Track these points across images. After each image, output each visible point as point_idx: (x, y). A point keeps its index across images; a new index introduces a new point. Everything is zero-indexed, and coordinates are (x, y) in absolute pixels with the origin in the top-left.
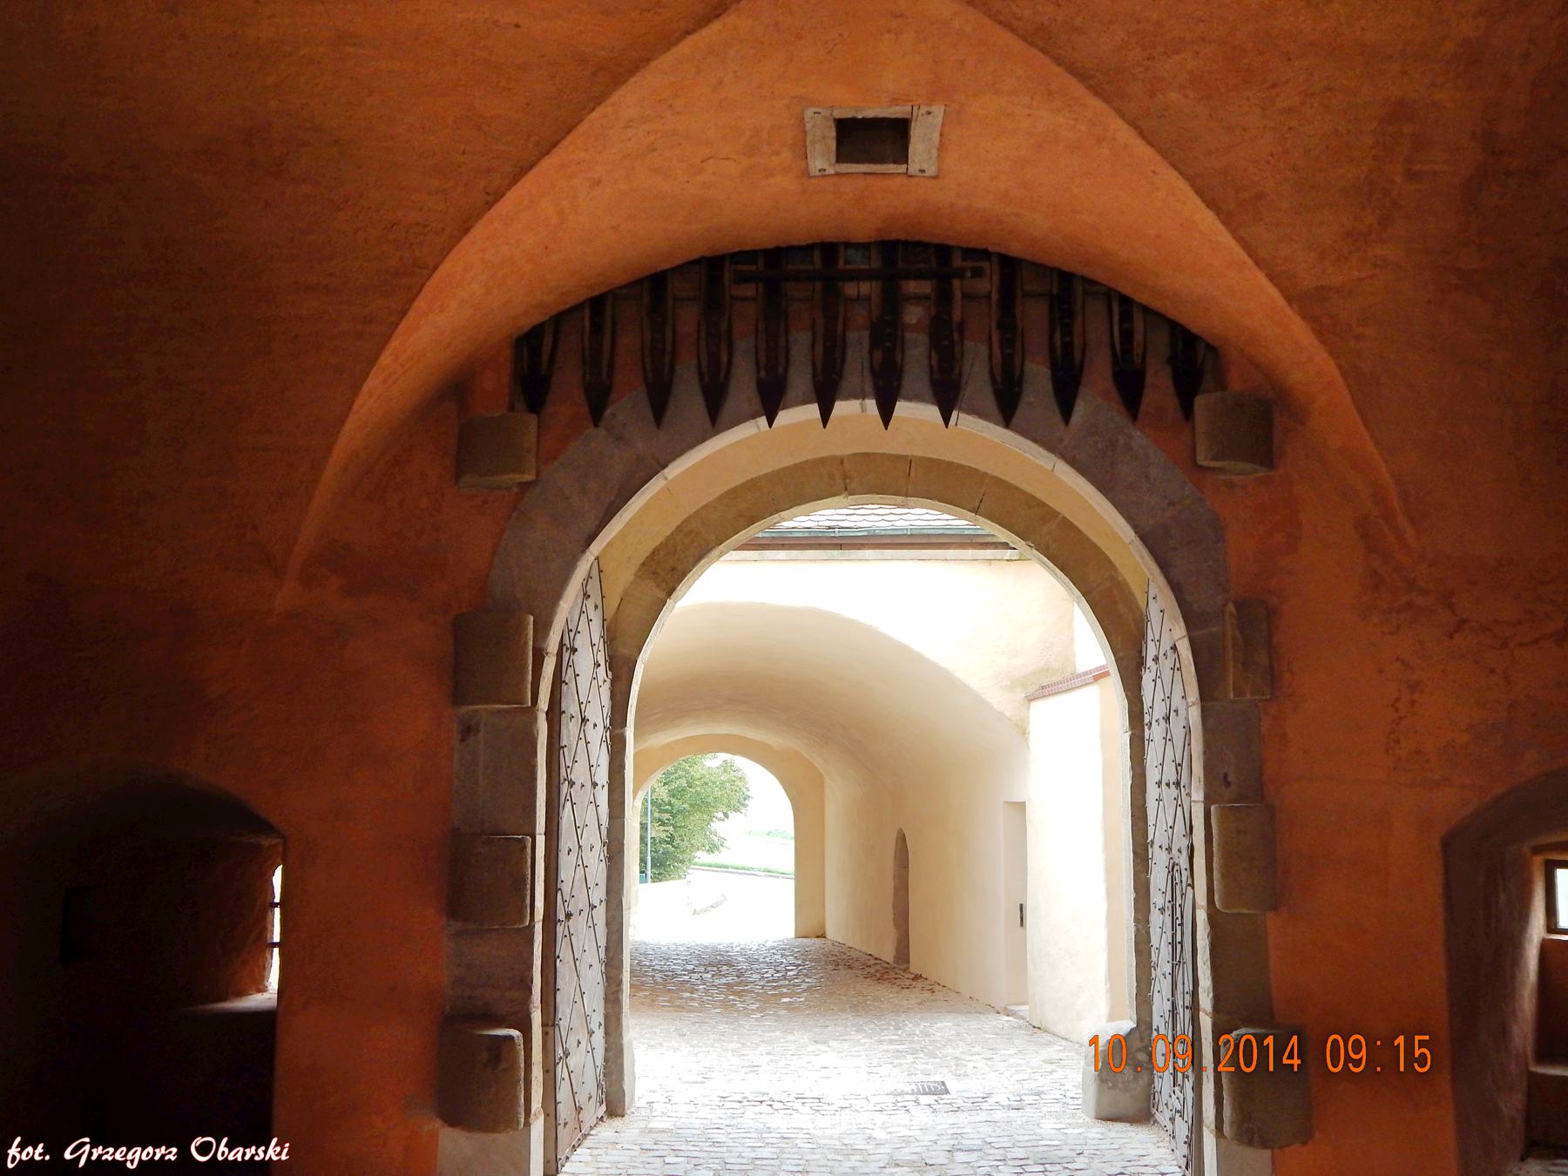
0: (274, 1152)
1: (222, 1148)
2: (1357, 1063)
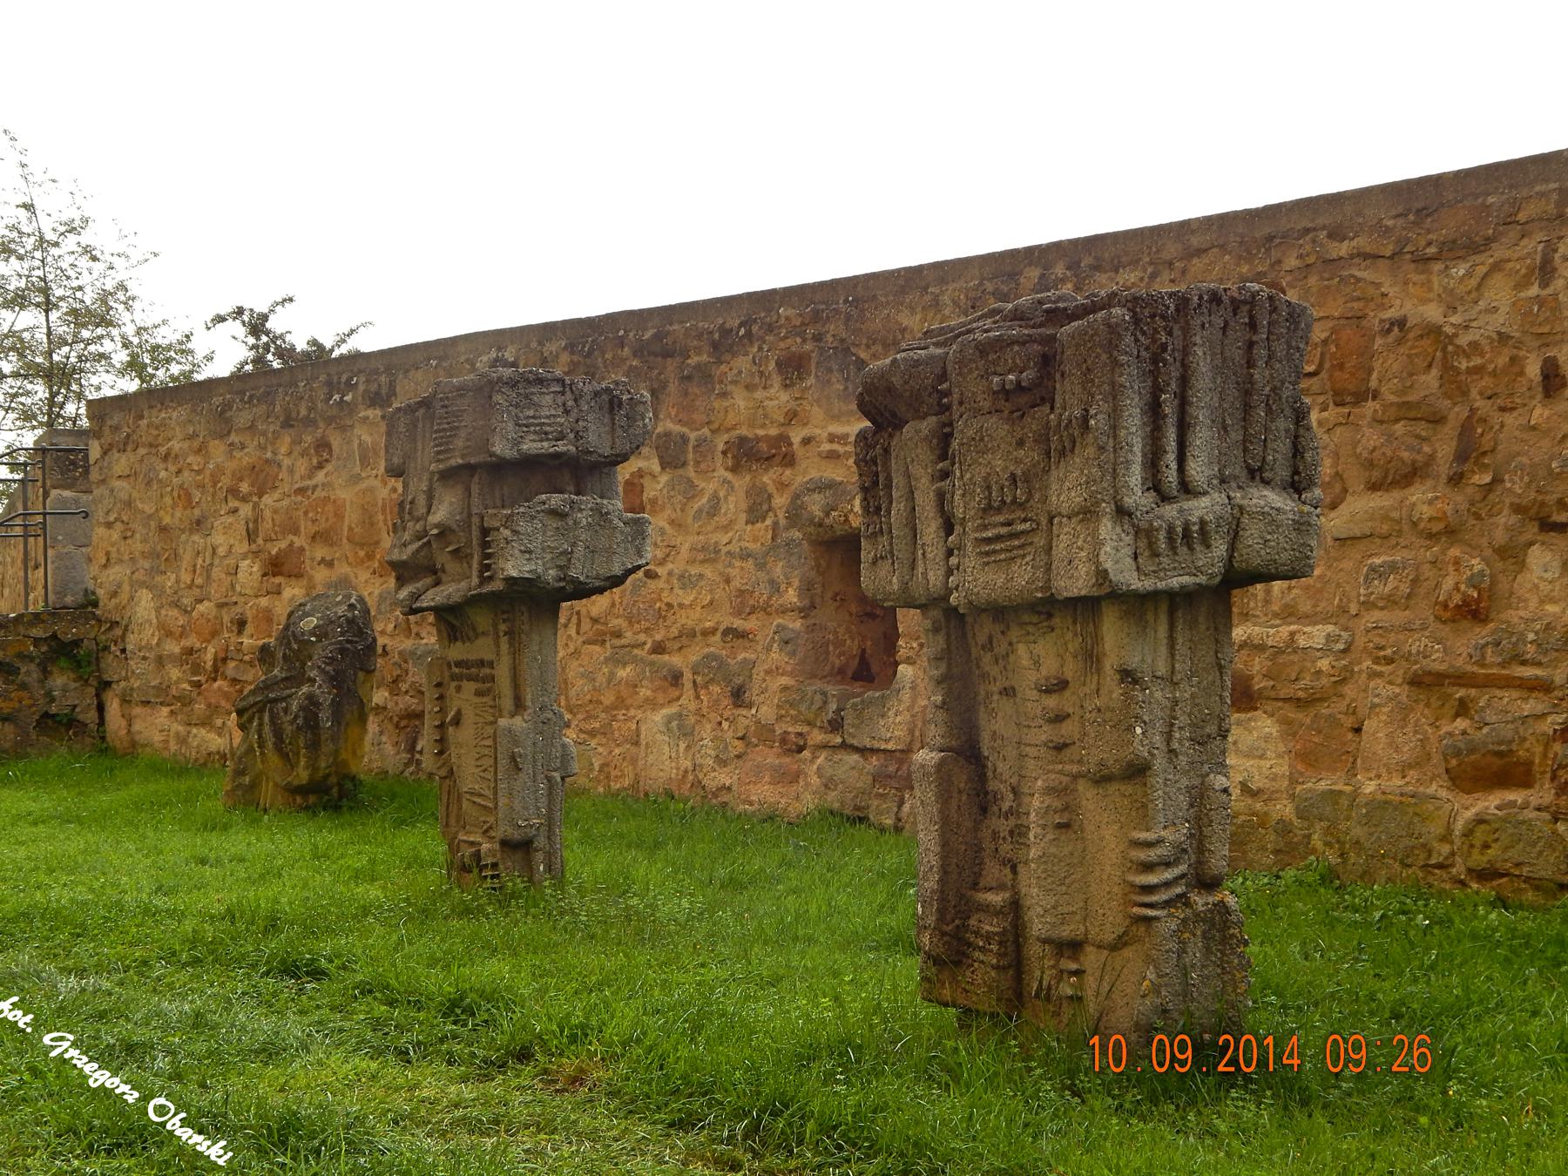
0: (216, 1152)
1: (176, 1120)
2: (1183, 1063)
